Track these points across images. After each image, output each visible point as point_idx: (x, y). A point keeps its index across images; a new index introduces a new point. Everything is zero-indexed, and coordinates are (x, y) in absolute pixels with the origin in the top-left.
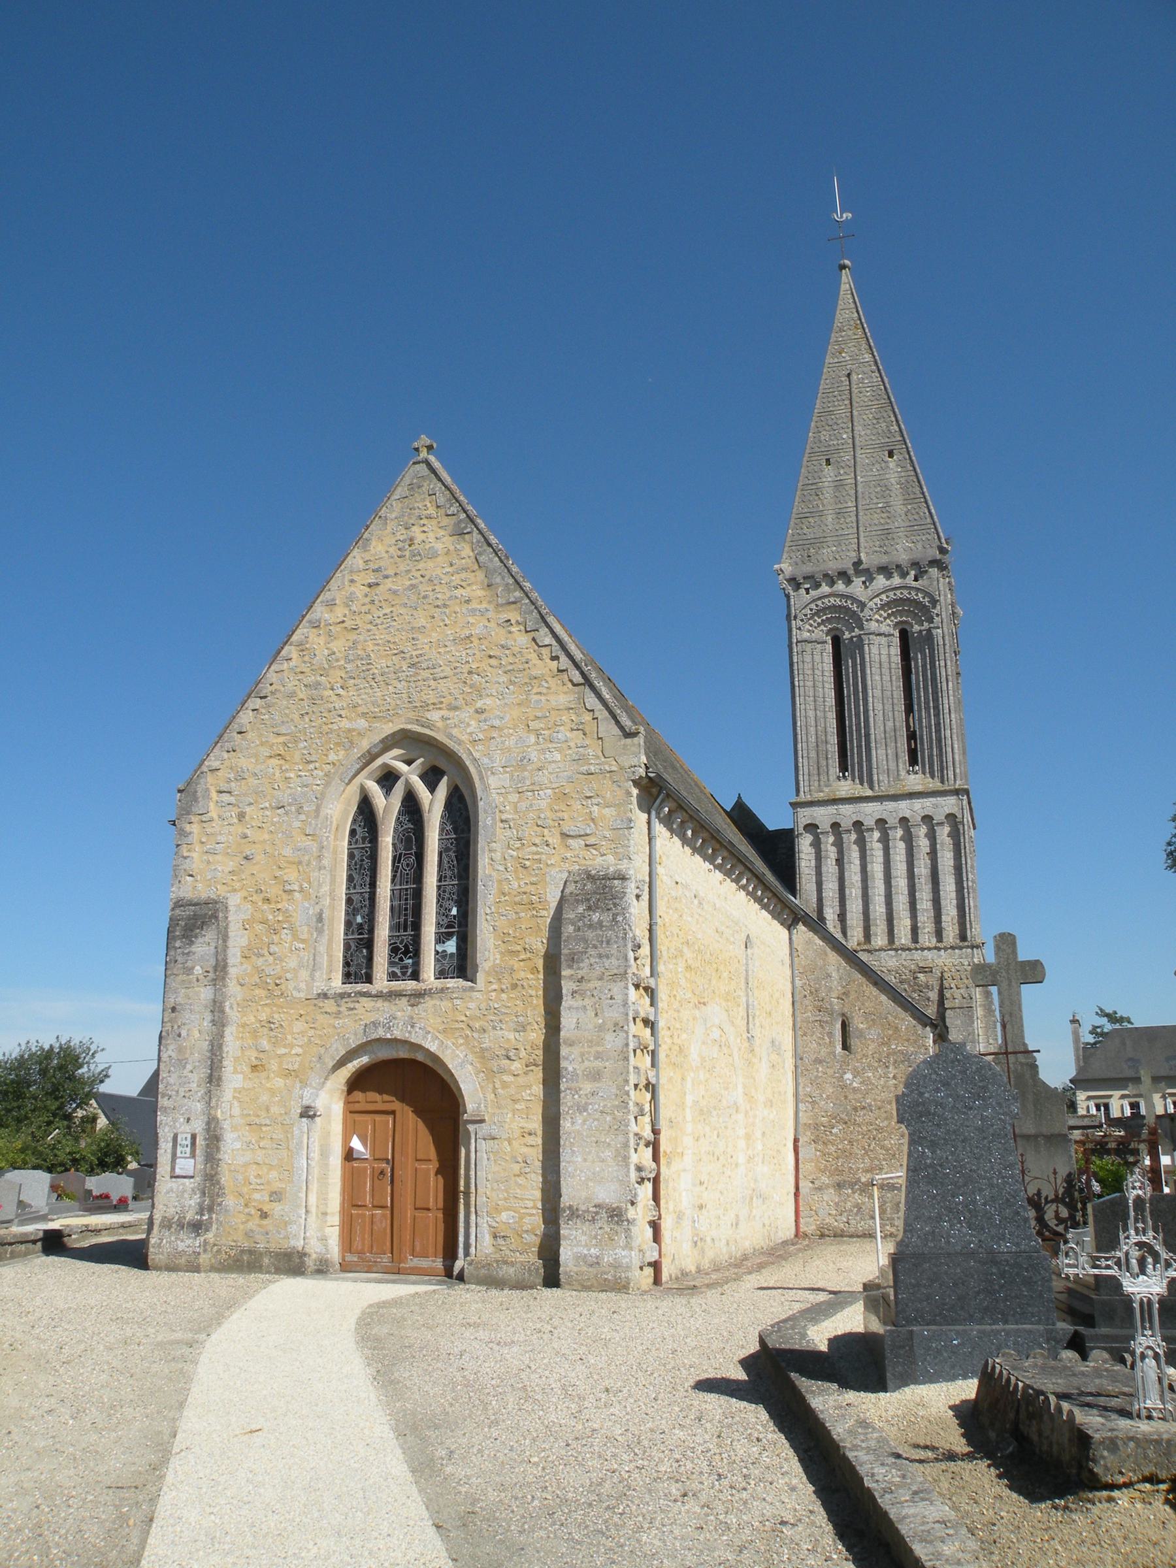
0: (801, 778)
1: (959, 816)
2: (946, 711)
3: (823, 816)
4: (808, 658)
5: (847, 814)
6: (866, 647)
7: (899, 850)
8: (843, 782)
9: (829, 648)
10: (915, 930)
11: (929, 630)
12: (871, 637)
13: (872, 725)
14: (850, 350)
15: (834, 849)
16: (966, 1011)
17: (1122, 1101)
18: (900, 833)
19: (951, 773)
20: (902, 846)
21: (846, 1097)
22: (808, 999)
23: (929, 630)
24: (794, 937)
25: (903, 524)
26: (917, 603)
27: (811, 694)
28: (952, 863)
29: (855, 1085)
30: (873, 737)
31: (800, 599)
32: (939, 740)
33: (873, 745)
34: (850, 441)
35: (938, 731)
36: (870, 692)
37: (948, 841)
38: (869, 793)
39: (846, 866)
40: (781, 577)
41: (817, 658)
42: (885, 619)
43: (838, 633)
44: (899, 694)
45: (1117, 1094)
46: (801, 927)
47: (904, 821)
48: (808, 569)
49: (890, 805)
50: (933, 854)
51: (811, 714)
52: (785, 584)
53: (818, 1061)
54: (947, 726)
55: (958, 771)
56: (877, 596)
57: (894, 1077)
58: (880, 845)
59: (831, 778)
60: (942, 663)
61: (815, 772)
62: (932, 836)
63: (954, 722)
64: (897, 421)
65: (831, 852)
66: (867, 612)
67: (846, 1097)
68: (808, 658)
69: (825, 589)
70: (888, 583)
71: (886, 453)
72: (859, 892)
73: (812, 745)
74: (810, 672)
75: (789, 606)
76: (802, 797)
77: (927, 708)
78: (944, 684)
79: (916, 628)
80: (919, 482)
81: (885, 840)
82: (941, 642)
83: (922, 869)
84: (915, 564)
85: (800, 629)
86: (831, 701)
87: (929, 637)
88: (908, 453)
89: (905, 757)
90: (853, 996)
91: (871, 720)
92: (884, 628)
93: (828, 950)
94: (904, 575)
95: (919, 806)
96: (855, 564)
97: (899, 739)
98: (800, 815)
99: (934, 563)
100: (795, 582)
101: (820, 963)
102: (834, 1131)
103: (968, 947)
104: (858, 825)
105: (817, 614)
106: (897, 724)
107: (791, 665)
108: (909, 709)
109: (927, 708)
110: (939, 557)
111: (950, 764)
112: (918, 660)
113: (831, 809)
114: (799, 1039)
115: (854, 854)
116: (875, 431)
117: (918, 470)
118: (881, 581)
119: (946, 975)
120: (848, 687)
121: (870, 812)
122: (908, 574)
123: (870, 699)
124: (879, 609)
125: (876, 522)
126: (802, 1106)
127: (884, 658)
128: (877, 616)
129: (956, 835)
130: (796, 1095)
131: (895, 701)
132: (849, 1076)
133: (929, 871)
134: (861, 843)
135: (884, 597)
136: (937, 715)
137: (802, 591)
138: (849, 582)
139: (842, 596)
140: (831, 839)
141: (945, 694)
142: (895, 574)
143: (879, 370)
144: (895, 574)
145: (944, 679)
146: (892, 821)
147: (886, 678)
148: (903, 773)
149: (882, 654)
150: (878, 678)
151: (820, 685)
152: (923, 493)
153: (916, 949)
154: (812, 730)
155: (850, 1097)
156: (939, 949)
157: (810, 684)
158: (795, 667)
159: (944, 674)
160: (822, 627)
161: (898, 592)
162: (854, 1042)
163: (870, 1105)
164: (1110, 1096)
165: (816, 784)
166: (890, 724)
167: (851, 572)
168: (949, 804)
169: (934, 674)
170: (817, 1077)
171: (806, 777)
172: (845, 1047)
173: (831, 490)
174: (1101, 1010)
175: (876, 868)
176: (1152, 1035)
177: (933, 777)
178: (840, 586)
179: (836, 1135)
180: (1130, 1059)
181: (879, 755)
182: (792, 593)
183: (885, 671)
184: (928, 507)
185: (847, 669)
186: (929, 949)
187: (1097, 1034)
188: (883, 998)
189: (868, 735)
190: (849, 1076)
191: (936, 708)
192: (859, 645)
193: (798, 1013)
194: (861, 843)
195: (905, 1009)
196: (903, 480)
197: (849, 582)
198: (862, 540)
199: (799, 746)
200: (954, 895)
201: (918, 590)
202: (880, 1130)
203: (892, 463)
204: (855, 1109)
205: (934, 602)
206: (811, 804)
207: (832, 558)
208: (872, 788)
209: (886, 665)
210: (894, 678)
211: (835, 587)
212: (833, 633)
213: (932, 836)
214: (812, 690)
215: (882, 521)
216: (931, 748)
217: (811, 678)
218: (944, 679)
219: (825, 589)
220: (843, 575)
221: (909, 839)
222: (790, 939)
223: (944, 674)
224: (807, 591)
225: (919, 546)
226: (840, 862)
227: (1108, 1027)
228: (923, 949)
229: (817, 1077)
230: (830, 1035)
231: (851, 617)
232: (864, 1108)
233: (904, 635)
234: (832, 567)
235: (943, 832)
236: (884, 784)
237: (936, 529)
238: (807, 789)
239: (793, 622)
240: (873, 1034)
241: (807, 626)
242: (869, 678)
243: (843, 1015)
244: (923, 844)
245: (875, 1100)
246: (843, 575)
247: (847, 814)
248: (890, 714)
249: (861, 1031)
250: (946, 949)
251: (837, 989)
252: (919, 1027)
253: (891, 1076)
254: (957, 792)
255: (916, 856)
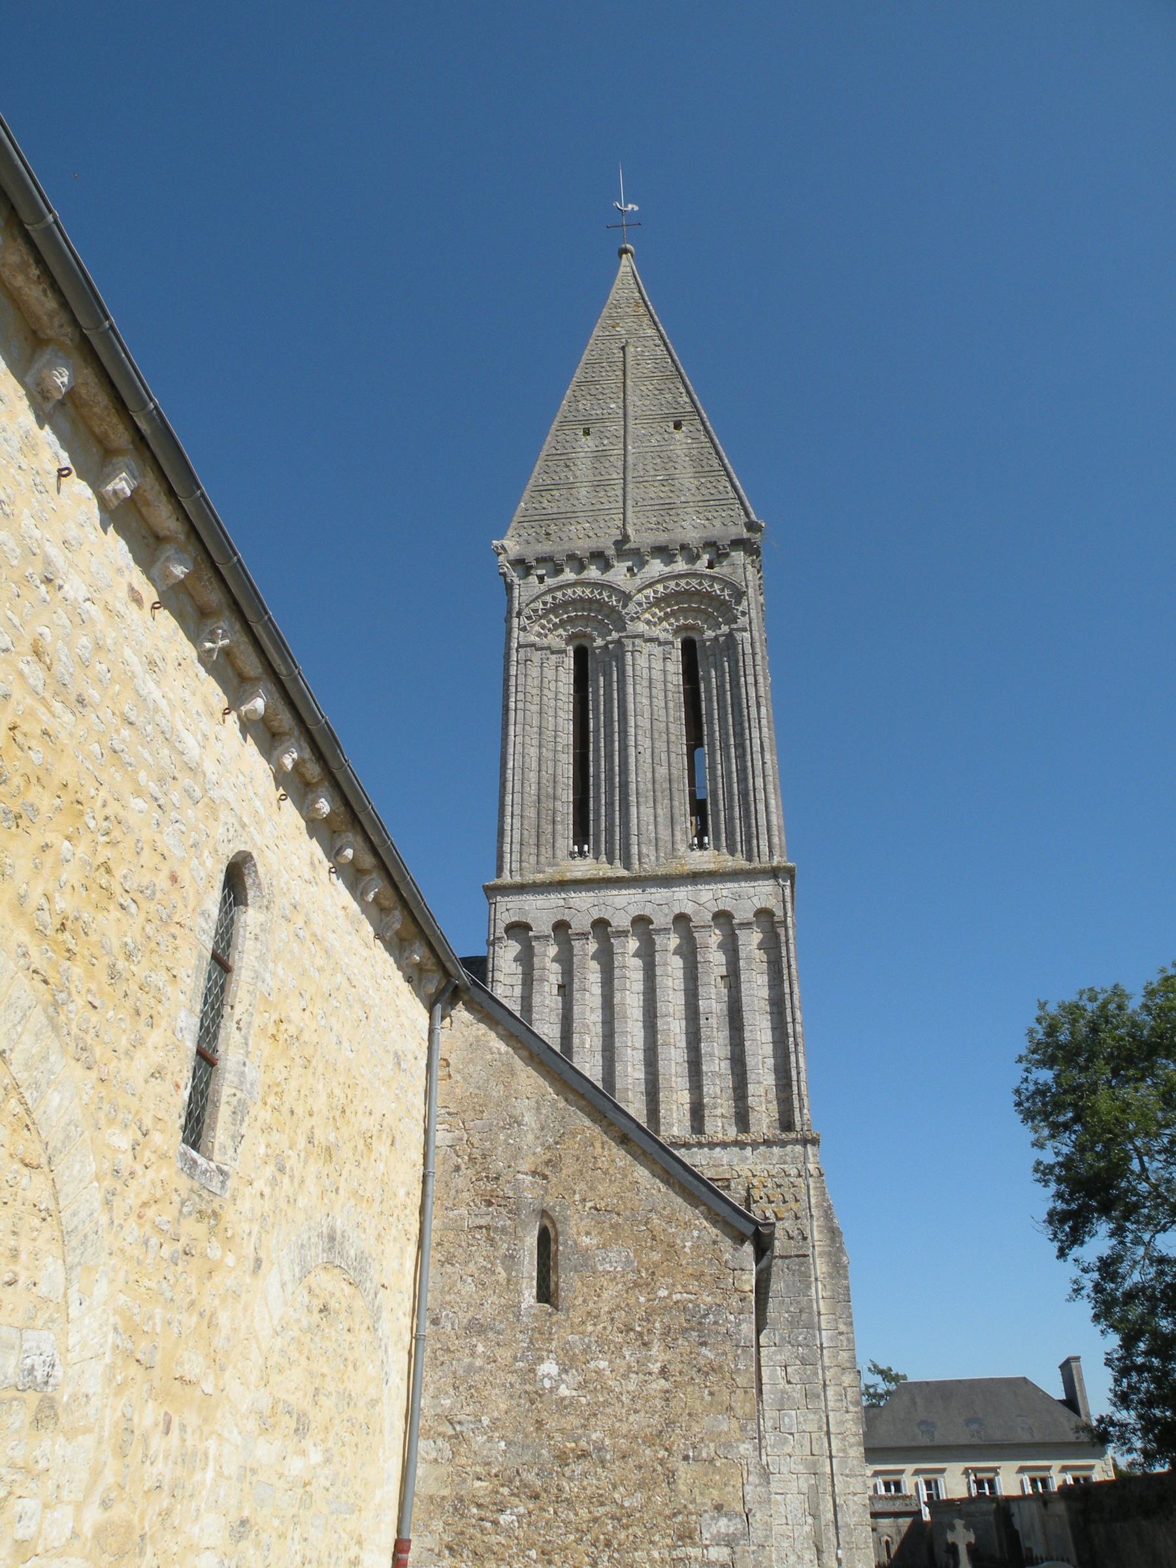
0: (507, 848)
1: (779, 913)
2: (757, 748)
3: (540, 911)
4: (534, 672)
5: (583, 907)
6: (629, 656)
7: (672, 970)
8: (578, 861)
9: (570, 662)
10: (697, 1112)
11: (730, 636)
12: (637, 641)
13: (632, 767)
14: (626, 320)
15: (556, 967)
16: (794, 1263)
17: (1021, 1476)
18: (674, 941)
19: (764, 844)
20: (677, 962)
21: (539, 1424)
22: (465, 1185)
23: (730, 636)
24: (443, 1036)
25: (693, 499)
26: (710, 597)
27: (535, 723)
28: (765, 993)
29: (564, 1391)
30: (633, 786)
31: (527, 589)
32: (744, 794)
33: (633, 798)
34: (621, 411)
35: (743, 780)
36: (632, 722)
37: (760, 955)
38: (623, 873)
39: (577, 995)
40: (501, 558)
41: (550, 674)
42: (661, 620)
43: (585, 642)
44: (679, 730)
45: (910, 1468)
46: (461, 1013)
47: (681, 920)
48: (545, 548)
49: (659, 894)
50: (733, 978)
51: (533, 751)
52: (507, 569)
53: (476, 1328)
54: (759, 771)
55: (776, 840)
56: (650, 585)
57: (664, 1372)
58: (638, 962)
59: (559, 853)
60: (751, 679)
61: (533, 841)
62: (731, 948)
63: (769, 765)
64: (688, 392)
65: (552, 974)
66: (632, 608)
67: (539, 1424)
68: (534, 672)
69: (569, 575)
70: (668, 569)
71: (671, 425)
72: (598, 1043)
73: (531, 798)
74: (535, 691)
75: (510, 601)
76: (506, 879)
77: (725, 748)
78: (753, 710)
79: (709, 634)
80: (717, 453)
81: (648, 954)
82: (748, 650)
83: (713, 1001)
84: (710, 545)
85: (524, 629)
86: (567, 736)
87: (730, 645)
88: (703, 424)
89: (686, 822)
90: (569, 1167)
91: (632, 760)
92: (656, 632)
93: (518, 1063)
94: (693, 558)
95: (710, 895)
96: (616, 543)
97: (676, 795)
98: (501, 908)
99: (737, 543)
100: (522, 566)
101: (497, 1092)
102: (505, 1519)
103: (796, 1142)
104: (601, 925)
105: (554, 609)
106: (674, 771)
107: (506, 680)
108: (695, 738)
109: (725, 748)
110: (745, 534)
111: (763, 829)
112: (710, 679)
113: (555, 900)
114: (432, 1271)
115: (591, 976)
116: (656, 402)
117: (717, 441)
118: (656, 567)
119: (756, 1194)
120: (596, 718)
121: (622, 906)
122: (698, 557)
123: (632, 731)
124: (651, 605)
125: (653, 495)
126: (424, 1446)
127: (657, 675)
128: (647, 616)
129: (772, 945)
130: (411, 1414)
131: (673, 738)
132: (549, 1367)
133: (725, 1006)
134: (606, 958)
135: (660, 587)
136: (741, 757)
137: (533, 579)
138: (606, 566)
139: (594, 585)
140: (553, 950)
141: (754, 724)
142: (679, 558)
143: (665, 344)
144: (679, 558)
145: (753, 702)
146: (661, 920)
147: (659, 702)
148: (682, 848)
149: (652, 675)
150: (645, 701)
151: (551, 712)
152: (724, 466)
153: (700, 1145)
154: (533, 776)
155: (551, 1424)
156: (741, 1145)
157: (535, 708)
158: (513, 682)
159: (752, 694)
160: (561, 631)
161: (683, 582)
162: (567, 1280)
163: (600, 1448)
164: (901, 1472)
165: (533, 859)
166: (662, 771)
167: (611, 552)
168: (763, 893)
169: (736, 698)
170: (470, 1369)
171: (516, 847)
172: (545, 1293)
173: (588, 462)
174: (875, 1366)
175: (631, 1001)
176: (944, 1391)
177: (732, 852)
178: (593, 573)
179: (509, 1532)
180: (923, 1422)
181: (642, 814)
182: (516, 581)
183: (658, 692)
184: (731, 481)
185: (596, 691)
186: (724, 1145)
187: (869, 1395)
188: (641, 1173)
189: (624, 785)
190: (549, 1367)
191: (740, 746)
192: (617, 653)
193: (433, 1209)
194: (606, 958)
195: (693, 1199)
196: (694, 452)
197: (606, 566)
198: (629, 514)
199: (509, 798)
200: (768, 1049)
201: (713, 578)
202: (622, 1518)
203: (679, 435)
204: (562, 1458)
205: (739, 595)
206: (521, 889)
207: (580, 537)
208: (627, 865)
209: (659, 686)
210: (671, 704)
211: (585, 575)
212: (577, 642)
213: (731, 948)
214: (536, 717)
215: (662, 495)
216: (731, 808)
217: (536, 699)
218: (753, 702)
219: (569, 575)
220: (600, 558)
221: (690, 953)
222: (431, 1031)
223: (752, 694)
224: (541, 579)
225: (717, 523)
226: (565, 989)
227: (882, 1387)
228: (712, 1145)
229: (470, 1369)
230: (511, 1260)
231: (607, 617)
232: (584, 1455)
233: (690, 649)
234: (582, 547)
235: (751, 941)
236: (649, 861)
237: (742, 503)
238: (515, 866)
239: (515, 621)
240: (614, 1260)
241: (537, 628)
242: (630, 698)
243: (544, 1213)
244: (714, 960)
245: (613, 1433)
246: (600, 558)
247: (583, 907)
248: (664, 756)
249: (585, 1255)
250: (755, 1145)
251: (532, 1151)
252: (726, 1244)
253: (655, 1368)
254: (774, 873)
255: (702, 978)
